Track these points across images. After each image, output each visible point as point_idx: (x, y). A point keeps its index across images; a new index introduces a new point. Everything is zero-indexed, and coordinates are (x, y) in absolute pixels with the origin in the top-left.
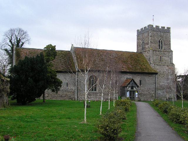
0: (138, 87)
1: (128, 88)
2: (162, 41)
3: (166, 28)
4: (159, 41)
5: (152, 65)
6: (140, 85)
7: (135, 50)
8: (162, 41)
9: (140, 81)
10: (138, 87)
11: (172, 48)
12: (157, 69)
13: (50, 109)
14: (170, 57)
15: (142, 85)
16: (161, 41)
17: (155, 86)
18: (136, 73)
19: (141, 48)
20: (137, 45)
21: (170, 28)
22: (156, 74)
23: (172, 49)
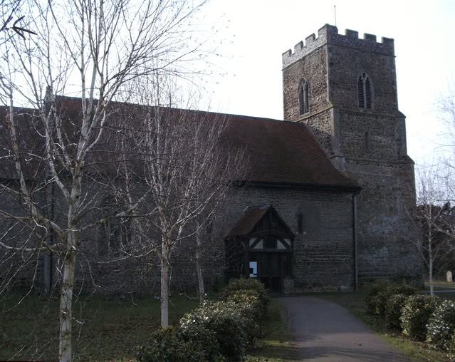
0: (292, 238)
1: (252, 241)
2: (368, 82)
3: (379, 40)
4: (361, 81)
5: (339, 163)
6: (301, 231)
7: (277, 114)
8: (368, 82)
9: (300, 218)
10: (292, 238)
11: (402, 107)
12: (359, 174)
13: (358, 98)
14: (397, 135)
15: (305, 233)
16: (364, 82)
17: (351, 237)
18: (350, 351)
19: (298, 108)
20: (285, 101)
21: (392, 40)
22: (356, 190)
23: (401, 108)
